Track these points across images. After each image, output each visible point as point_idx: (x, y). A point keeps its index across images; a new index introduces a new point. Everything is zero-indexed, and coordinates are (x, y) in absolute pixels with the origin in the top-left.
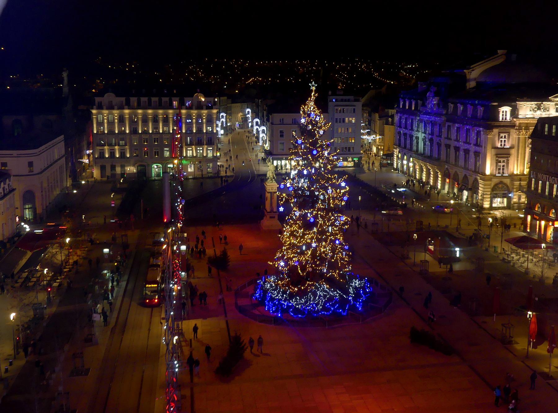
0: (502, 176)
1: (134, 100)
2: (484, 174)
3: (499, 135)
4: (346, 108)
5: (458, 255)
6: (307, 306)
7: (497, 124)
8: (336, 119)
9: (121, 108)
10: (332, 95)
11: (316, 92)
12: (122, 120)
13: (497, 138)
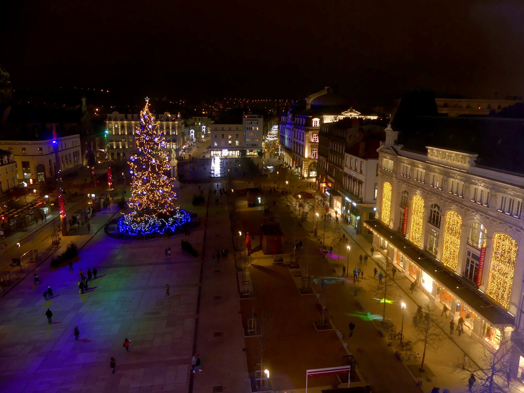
2: (304, 158)
5: (260, 202)
6: (9, 214)
7: (311, 128)
9: (122, 120)
10: (245, 114)
12: (123, 127)
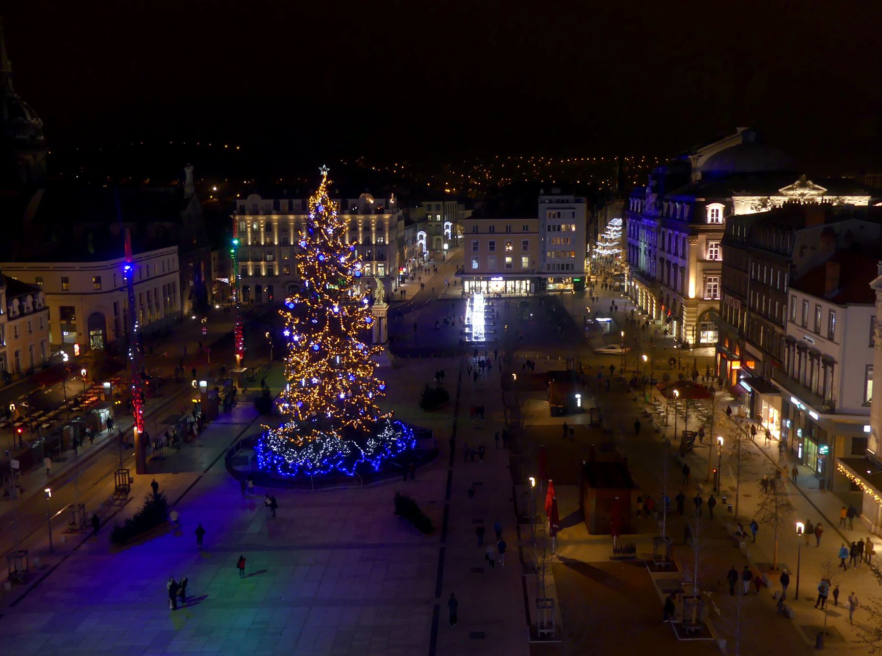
0: (713, 300)
1: (284, 203)
2: (687, 297)
3: (707, 244)
4: (561, 211)
5: (579, 405)
7: (703, 227)
8: (549, 226)
9: (268, 213)
11: (328, 178)
12: (269, 228)
13: (704, 247)
